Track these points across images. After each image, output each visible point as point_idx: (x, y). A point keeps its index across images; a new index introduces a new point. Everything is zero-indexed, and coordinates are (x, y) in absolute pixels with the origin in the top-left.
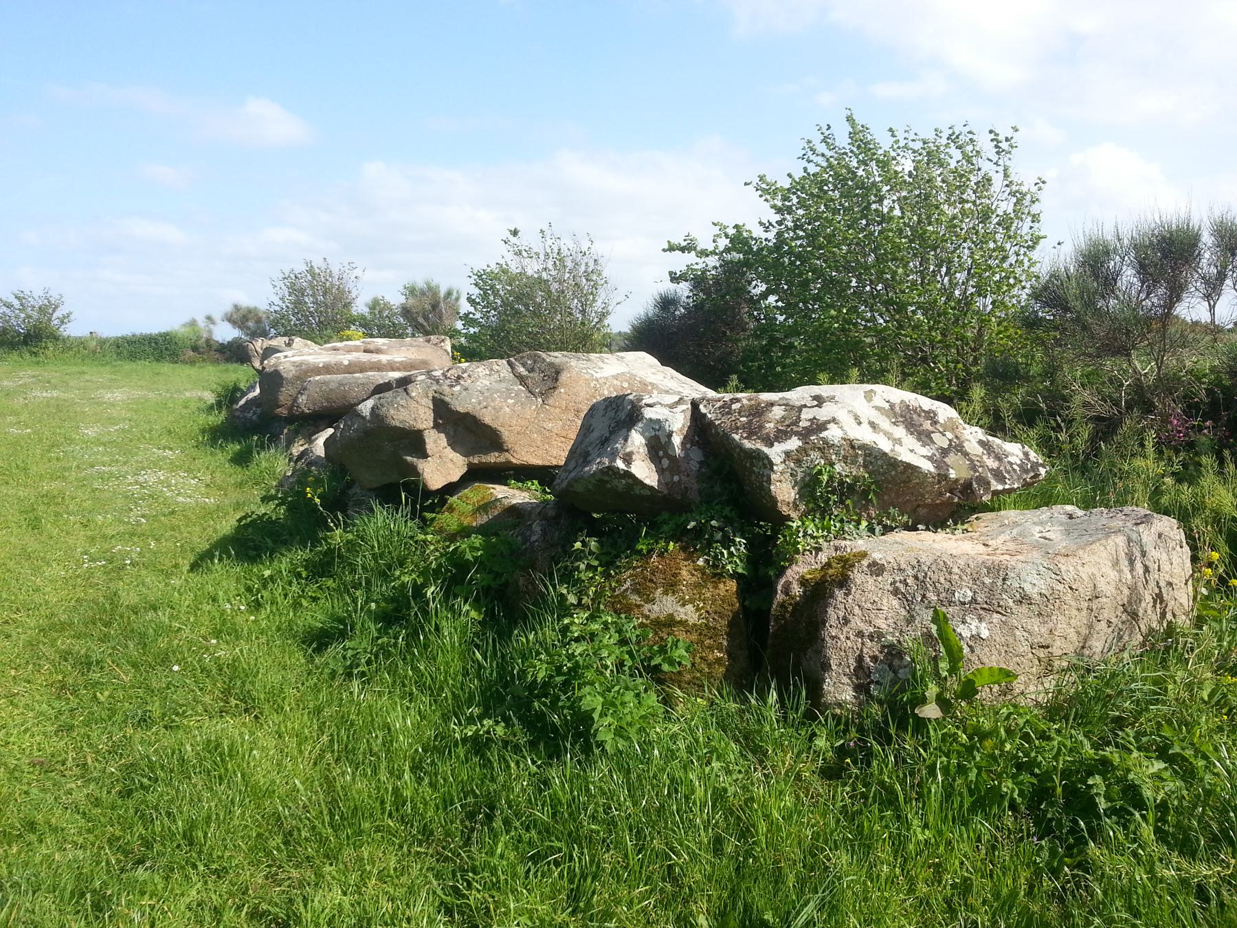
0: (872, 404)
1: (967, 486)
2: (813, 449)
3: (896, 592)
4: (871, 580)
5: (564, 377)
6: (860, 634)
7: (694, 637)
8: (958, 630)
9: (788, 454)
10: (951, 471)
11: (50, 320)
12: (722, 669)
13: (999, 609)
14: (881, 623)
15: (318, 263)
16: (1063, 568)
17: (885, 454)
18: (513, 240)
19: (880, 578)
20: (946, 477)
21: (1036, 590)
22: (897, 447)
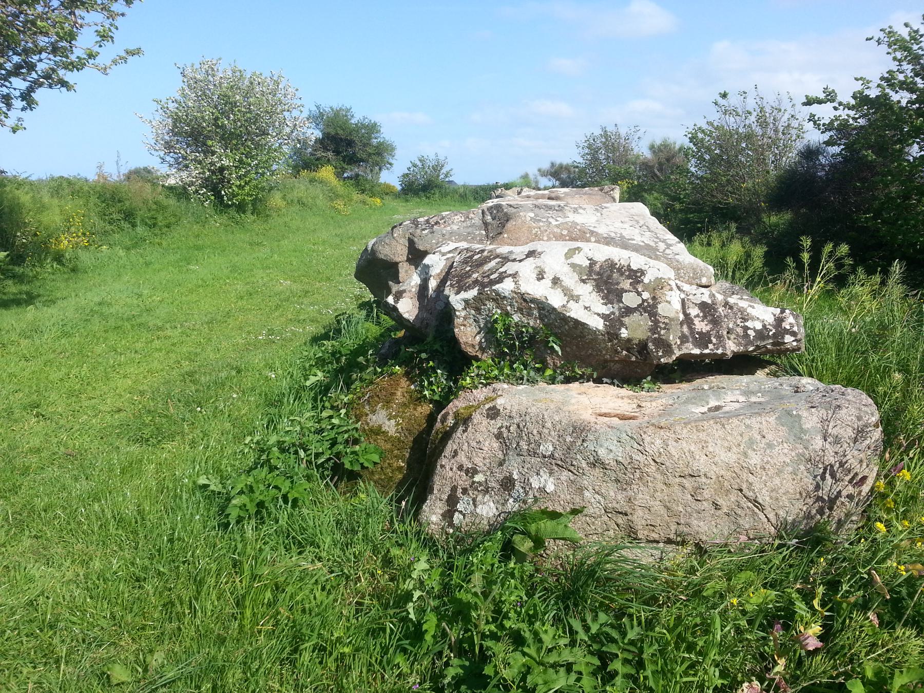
0: (569, 261)
1: (643, 346)
2: (488, 299)
3: (499, 436)
4: (485, 422)
5: (509, 225)
6: (460, 468)
7: (389, 446)
8: (531, 480)
9: (466, 301)
10: (623, 330)
11: (438, 176)
12: (400, 476)
13: (572, 468)
14: (478, 461)
15: (610, 129)
16: (647, 439)
17: (554, 309)
18: (721, 101)
19: (493, 421)
20: (617, 336)
21: (611, 456)
22: (572, 304)
